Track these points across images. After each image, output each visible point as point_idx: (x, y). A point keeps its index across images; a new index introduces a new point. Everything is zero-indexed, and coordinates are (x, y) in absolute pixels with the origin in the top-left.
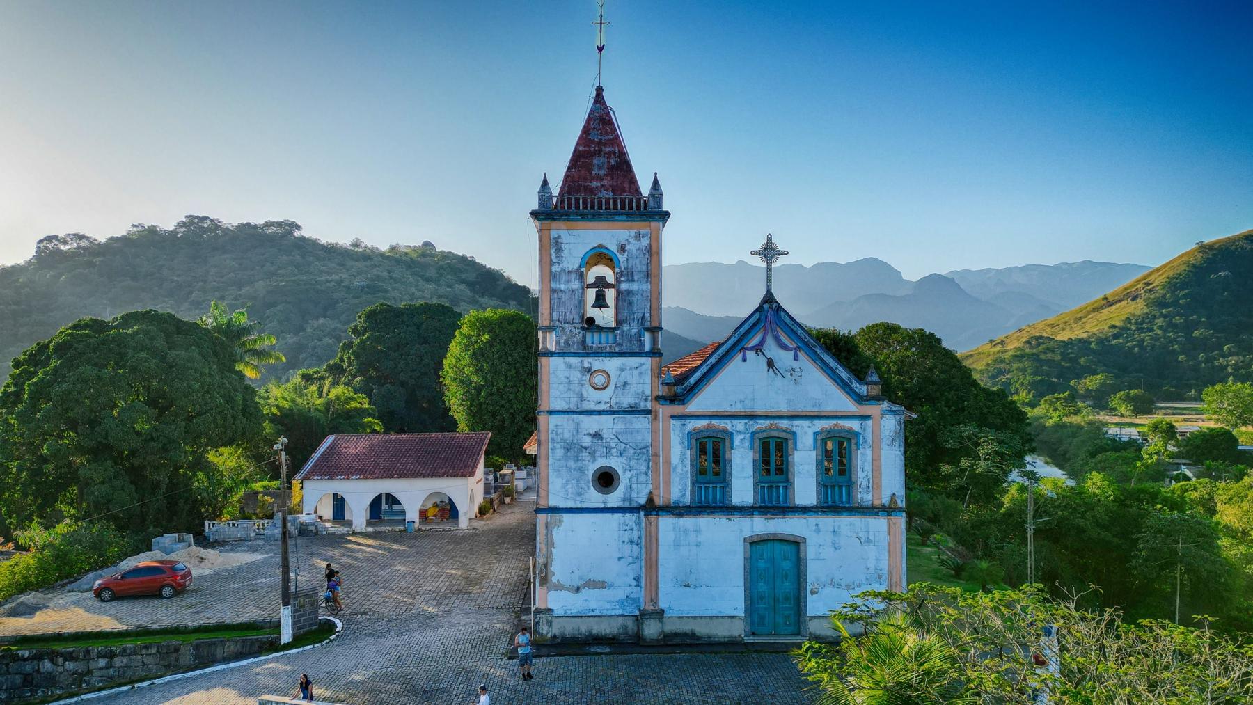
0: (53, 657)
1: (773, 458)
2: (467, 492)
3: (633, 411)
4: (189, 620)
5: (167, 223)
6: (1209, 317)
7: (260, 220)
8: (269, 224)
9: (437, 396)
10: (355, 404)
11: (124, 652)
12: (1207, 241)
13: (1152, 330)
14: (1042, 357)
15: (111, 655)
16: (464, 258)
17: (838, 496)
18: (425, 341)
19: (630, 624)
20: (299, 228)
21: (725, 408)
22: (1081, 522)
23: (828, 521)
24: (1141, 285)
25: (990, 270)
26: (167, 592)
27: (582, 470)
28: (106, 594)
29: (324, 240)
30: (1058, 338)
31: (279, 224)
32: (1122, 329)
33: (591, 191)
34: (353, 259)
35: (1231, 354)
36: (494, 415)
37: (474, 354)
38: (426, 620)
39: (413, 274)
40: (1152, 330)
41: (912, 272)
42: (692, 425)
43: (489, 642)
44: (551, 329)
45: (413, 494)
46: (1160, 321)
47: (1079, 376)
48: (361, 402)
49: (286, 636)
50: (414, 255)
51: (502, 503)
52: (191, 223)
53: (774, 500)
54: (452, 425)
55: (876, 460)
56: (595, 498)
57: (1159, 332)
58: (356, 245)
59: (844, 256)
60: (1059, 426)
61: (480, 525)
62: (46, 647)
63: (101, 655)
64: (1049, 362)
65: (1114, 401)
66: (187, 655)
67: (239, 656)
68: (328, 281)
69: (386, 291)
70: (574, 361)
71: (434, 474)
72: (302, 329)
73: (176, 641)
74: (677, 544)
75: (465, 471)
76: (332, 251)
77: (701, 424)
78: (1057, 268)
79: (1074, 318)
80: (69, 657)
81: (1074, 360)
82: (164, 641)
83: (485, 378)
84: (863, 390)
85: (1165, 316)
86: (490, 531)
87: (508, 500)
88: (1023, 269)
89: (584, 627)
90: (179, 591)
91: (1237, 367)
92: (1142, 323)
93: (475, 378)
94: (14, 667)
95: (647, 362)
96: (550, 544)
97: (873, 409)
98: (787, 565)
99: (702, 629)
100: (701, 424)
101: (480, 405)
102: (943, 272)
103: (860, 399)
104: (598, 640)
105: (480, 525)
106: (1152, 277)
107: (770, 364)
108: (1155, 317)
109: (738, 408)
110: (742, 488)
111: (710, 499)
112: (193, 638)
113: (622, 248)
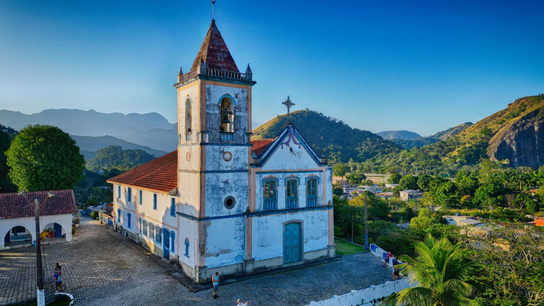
1: (292, 187)
3: (241, 170)
12: (280, 115)
19: (239, 267)
24: (260, 129)
27: (220, 199)
42: (265, 176)
56: (225, 211)
70: (217, 147)
74: (259, 229)
77: (267, 175)
95: (247, 148)
98: (296, 232)
99: (268, 264)
100: (267, 175)
107: (291, 150)
109: (280, 169)
111: (270, 209)
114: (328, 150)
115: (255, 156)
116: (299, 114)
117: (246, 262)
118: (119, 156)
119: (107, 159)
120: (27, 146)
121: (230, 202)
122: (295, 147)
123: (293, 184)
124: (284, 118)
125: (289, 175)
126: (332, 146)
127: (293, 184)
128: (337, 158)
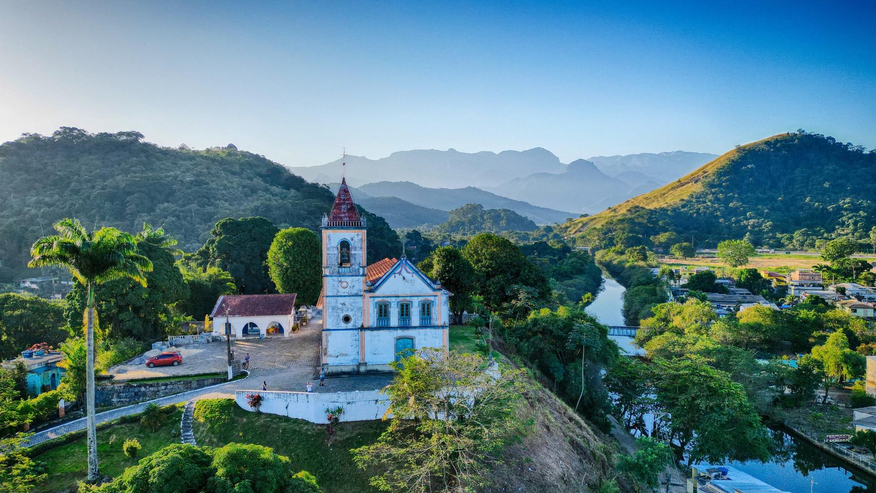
0: (145, 386)
1: (405, 311)
2: (287, 321)
3: (356, 295)
5: (47, 132)
6: (739, 194)
7: (113, 131)
8: (121, 134)
10: (223, 277)
11: (171, 383)
12: (742, 144)
14: (636, 220)
15: (166, 385)
16: (257, 156)
17: (426, 323)
18: (254, 240)
19: (355, 367)
20: (142, 136)
21: (388, 294)
22: (551, 328)
24: (701, 173)
25: (617, 157)
26: (176, 363)
27: (338, 316)
28: (152, 365)
29: (160, 145)
30: (647, 207)
31: (129, 134)
32: (688, 201)
33: (341, 218)
34: (181, 159)
35: (751, 218)
36: (295, 281)
37: (284, 251)
38: (281, 370)
39: (224, 170)
41: (566, 158)
42: (377, 300)
43: (306, 376)
44: (327, 267)
45: (264, 323)
46: (710, 197)
47: (657, 233)
48: (227, 275)
49: (230, 376)
50: (224, 155)
51: (302, 325)
52: (65, 132)
53: (405, 325)
54: (272, 288)
56: (343, 325)
57: (709, 204)
58: (182, 148)
60: (633, 267)
61: (294, 335)
62: (142, 383)
63: (163, 385)
64: (639, 224)
65: (673, 249)
66: (194, 385)
68: (167, 176)
69: (208, 184)
70: (336, 278)
71: (272, 314)
72: (154, 211)
73: (190, 379)
75: (286, 312)
77: (380, 299)
78: (660, 156)
79: (664, 194)
80: (151, 386)
81: (655, 223)
82: (185, 379)
83: (290, 264)
84: (435, 286)
85: (714, 194)
86: (300, 338)
87: (304, 324)
89: (339, 369)
90: (180, 363)
91: (753, 226)
93: (285, 264)
94: (131, 390)
95: (362, 279)
96: (327, 341)
97: (439, 293)
99: (380, 368)
100: (380, 299)
101: (287, 277)
102: (586, 157)
103: (434, 290)
105: (294, 335)
107: (404, 278)
108: (707, 194)
109: (393, 294)
110: (394, 320)
111: (383, 324)
112: (196, 378)
113: (352, 239)
114: (839, 209)
116: (781, 142)
117: (360, 364)
118: (479, 219)
119: (463, 224)
121: (347, 319)
123: (428, 305)
124: (749, 150)
126: (848, 200)
127: (385, 306)
128: (855, 224)
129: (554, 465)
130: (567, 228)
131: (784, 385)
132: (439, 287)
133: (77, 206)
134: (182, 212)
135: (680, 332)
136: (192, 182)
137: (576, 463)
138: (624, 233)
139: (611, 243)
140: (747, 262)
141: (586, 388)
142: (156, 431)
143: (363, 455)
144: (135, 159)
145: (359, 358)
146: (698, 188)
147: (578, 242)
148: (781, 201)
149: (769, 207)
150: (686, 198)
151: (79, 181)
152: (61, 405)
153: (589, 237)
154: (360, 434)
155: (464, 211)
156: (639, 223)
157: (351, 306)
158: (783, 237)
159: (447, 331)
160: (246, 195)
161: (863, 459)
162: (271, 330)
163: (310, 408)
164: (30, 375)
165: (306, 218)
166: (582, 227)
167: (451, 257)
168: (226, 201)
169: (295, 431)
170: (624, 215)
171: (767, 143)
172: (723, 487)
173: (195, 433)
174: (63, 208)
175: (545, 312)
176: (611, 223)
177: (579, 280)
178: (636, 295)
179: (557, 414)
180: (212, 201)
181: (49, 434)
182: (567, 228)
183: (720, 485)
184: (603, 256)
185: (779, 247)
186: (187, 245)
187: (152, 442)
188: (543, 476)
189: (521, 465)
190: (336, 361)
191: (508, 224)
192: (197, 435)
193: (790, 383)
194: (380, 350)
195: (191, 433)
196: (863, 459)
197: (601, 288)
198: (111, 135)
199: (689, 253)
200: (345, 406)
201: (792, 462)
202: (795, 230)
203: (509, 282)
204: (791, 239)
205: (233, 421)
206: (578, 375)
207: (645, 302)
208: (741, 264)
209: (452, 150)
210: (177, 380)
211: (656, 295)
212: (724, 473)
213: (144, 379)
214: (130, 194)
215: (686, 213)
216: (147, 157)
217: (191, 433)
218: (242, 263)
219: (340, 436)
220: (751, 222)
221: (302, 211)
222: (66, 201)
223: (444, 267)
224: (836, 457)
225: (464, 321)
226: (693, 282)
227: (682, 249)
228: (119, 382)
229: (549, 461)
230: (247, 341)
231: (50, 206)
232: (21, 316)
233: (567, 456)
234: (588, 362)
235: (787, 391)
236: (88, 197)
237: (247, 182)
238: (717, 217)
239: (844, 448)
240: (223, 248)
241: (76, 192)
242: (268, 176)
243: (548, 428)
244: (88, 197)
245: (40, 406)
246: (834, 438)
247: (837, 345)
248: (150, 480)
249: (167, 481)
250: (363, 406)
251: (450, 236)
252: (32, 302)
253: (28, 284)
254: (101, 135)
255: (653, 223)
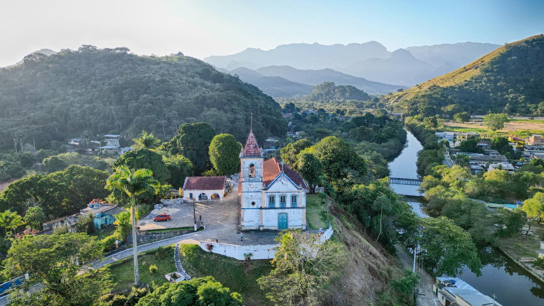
0: (155, 233)
1: (283, 199)
4: (172, 227)
6: (505, 77)
8: (117, 49)
9: (209, 162)
12: (509, 42)
13: (481, 82)
20: (129, 50)
22: (364, 197)
23: (292, 210)
24: (480, 62)
25: (426, 46)
30: (441, 86)
31: (121, 49)
32: (469, 82)
34: (152, 64)
35: (511, 93)
40: (481, 82)
41: (391, 48)
42: (268, 194)
45: (209, 193)
46: (485, 79)
47: (446, 105)
49: (196, 229)
50: (176, 60)
52: (85, 48)
55: (301, 200)
56: (251, 206)
57: (484, 83)
59: (361, 40)
61: (224, 199)
66: (178, 233)
67: (187, 233)
68: (145, 77)
69: (168, 81)
71: (214, 189)
72: (139, 99)
73: (176, 230)
74: (266, 214)
76: (143, 60)
79: (454, 73)
80: (158, 234)
81: (446, 97)
84: (299, 187)
85: (487, 76)
88: (442, 45)
89: (250, 228)
91: (512, 99)
92: (477, 79)
97: (300, 191)
98: (285, 217)
99: (270, 228)
103: (298, 189)
104: (252, 230)
105: (225, 199)
106: (485, 59)
108: (483, 77)
110: (277, 204)
111: (272, 206)
115: (265, 185)
116: (536, 41)
118: (332, 92)
119: (322, 95)
120: (216, 146)
122: (285, 182)
124: (514, 47)
125: (281, 194)
129: (358, 284)
130: (389, 99)
131: (503, 223)
132: (301, 187)
133: (96, 95)
134: (155, 100)
135: (446, 185)
136: (159, 81)
137: (371, 281)
138: (424, 105)
139: (415, 112)
140: (503, 127)
141: (382, 231)
142: (163, 259)
143: (262, 281)
144: (126, 65)
145: (260, 223)
146: (476, 73)
147: (395, 110)
148: (533, 82)
149: (524, 85)
150: (468, 79)
151: (95, 80)
152: (117, 242)
153: (402, 106)
154: (261, 267)
155: (322, 87)
156: (435, 98)
157: (256, 197)
158: (532, 106)
159: (305, 210)
160: (191, 88)
161: (538, 273)
162: (213, 196)
163: (236, 252)
164: (96, 219)
165: (226, 104)
166: (398, 99)
167: (309, 158)
168: (179, 92)
169: (229, 264)
170: (426, 91)
171: (527, 42)
172: (451, 291)
173: (182, 261)
174: (88, 97)
175: (362, 186)
176: (417, 98)
177: (391, 142)
178: (425, 156)
179: (363, 251)
180: (172, 93)
181: (113, 258)
182: (389, 99)
183: (449, 290)
184: (409, 121)
185: (527, 113)
186: (159, 121)
187: (162, 265)
188: (351, 290)
189: (340, 285)
190: (248, 224)
191: (350, 95)
192: (183, 263)
193: (507, 223)
194: (270, 219)
195: (179, 261)
196: (538, 273)
197: (406, 145)
198: (111, 50)
199: (466, 119)
200: (253, 252)
201: (504, 267)
202: (540, 101)
203: (342, 167)
204: (536, 108)
205: (199, 257)
206: (378, 223)
207: (430, 161)
208: (499, 129)
209: (316, 44)
210: (170, 231)
211: (437, 156)
212: (453, 283)
213: (154, 230)
214: (125, 88)
215: (467, 90)
216: (133, 64)
217: (179, 261)
218: (194, 150)
219: (251, 267)
220: (511, 96)
221: (223, 100)
222: (89, 92)
223: (305, 164)
224: (524, 270)
225: (316, 192)
226: (463, 146)
227: (461, 116)
228: (143, 231)
229: (355, 281)
230: (201, 203)
231: (80, 95)
232: (82, 179)
233: (366, 277)
234: (385, 216)
235: (505, 227)
236: (102, 90)
237: (191, 79)
238: (488, 92)
239: (529, 266)
240: (185, 142)
241: (95, 87)
242: (202, 74)
243: (357, 262)
244: (102, 90)
245: (107, 244)
246: (524, 259)
247: (540, 200)
248: (172, 301)
249: (179, 302)
250: (262, 252)
251: (313, 104)
252: (87, 170)
253: (72, 143)
254: (106, 49)
255: (444, 97)
